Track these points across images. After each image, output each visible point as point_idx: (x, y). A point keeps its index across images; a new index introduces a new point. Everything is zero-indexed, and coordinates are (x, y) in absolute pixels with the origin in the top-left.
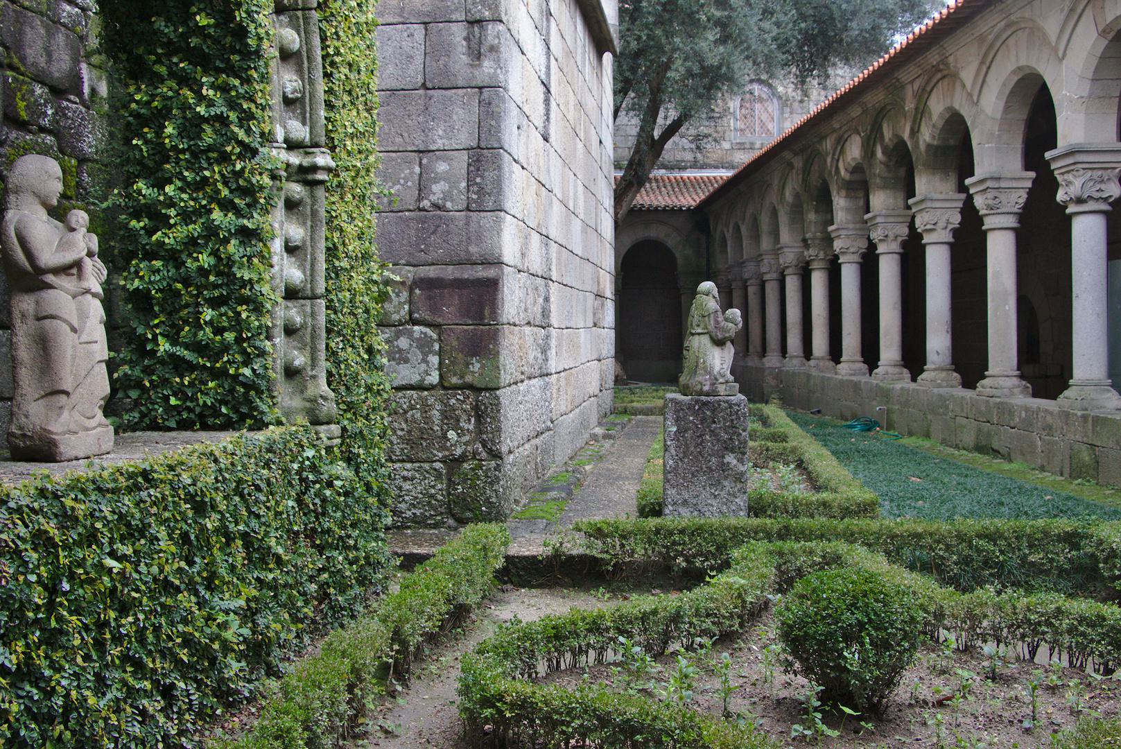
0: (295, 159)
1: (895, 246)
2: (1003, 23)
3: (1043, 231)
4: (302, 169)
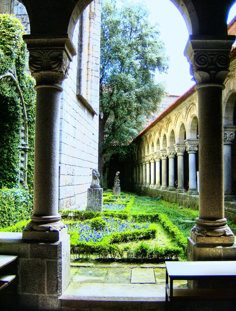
0: (23, 147)
2: (178, 112)
3: (186, 156)
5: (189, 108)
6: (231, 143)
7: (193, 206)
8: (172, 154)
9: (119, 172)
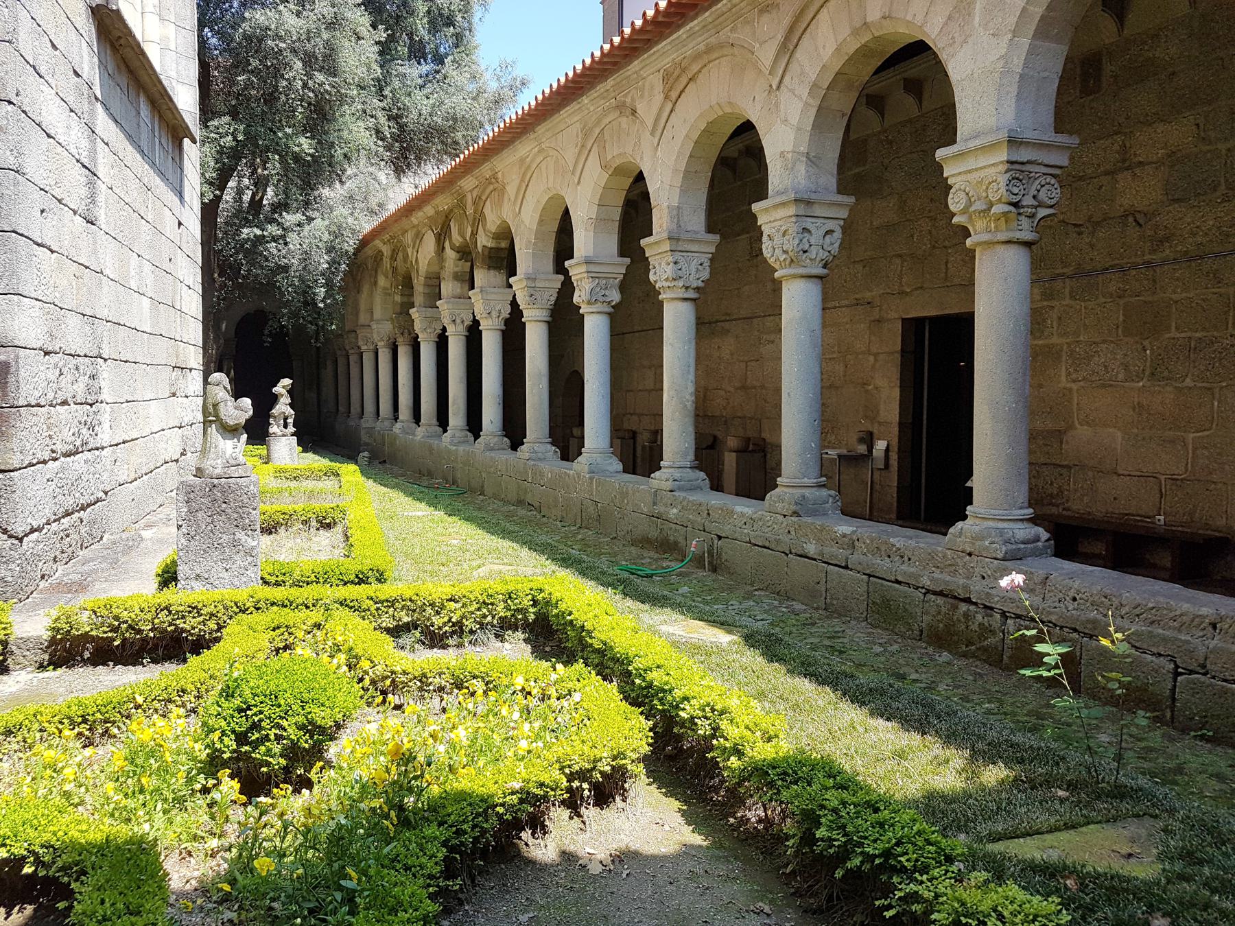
1: (544, 315)
3: (565, 323)
6: (826, 271)
8: (494, 314)
9: (287, 382)
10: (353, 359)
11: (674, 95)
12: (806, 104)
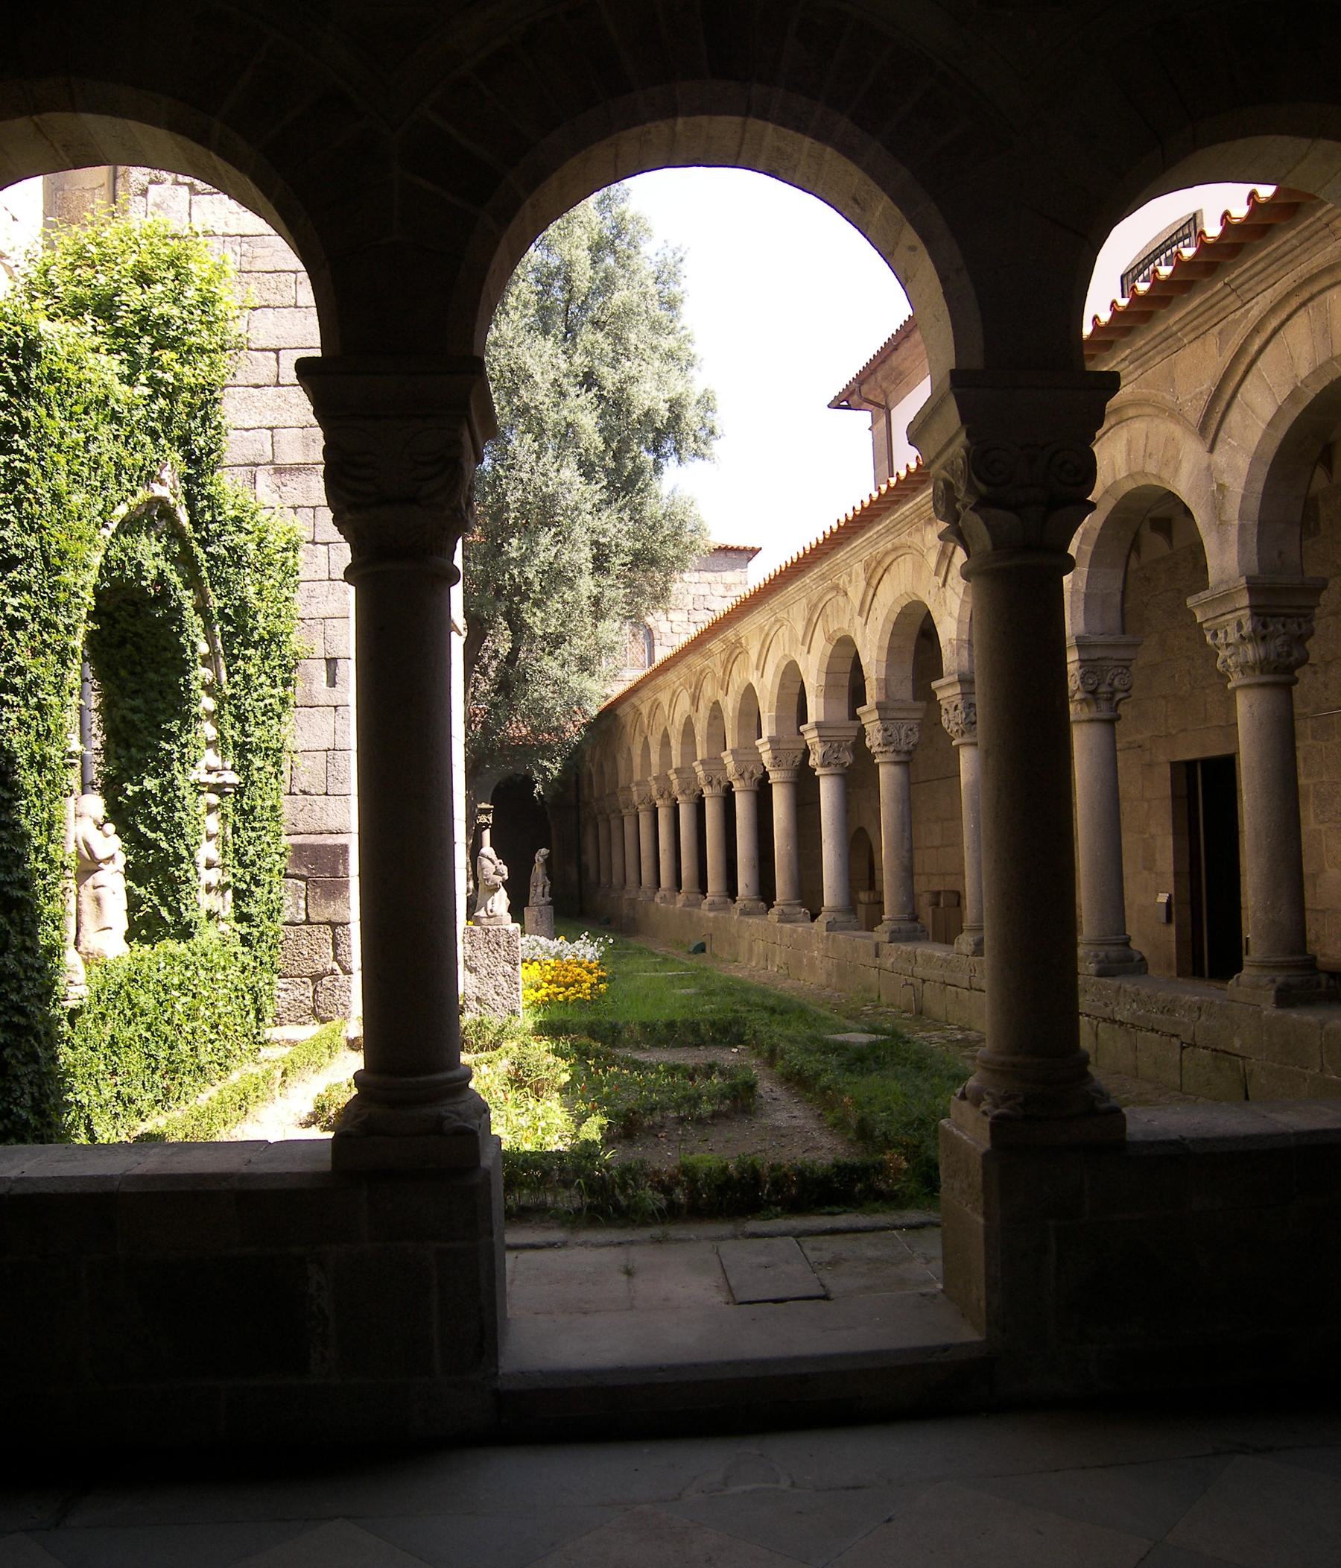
3: (857, 778)
4: (217, 785)
5: (821, 606)
7: (198, 788)
8: (747, 775)
9: (544, 851)
10: (615, 823)
11: (874, 582)
12: (963, 601)
